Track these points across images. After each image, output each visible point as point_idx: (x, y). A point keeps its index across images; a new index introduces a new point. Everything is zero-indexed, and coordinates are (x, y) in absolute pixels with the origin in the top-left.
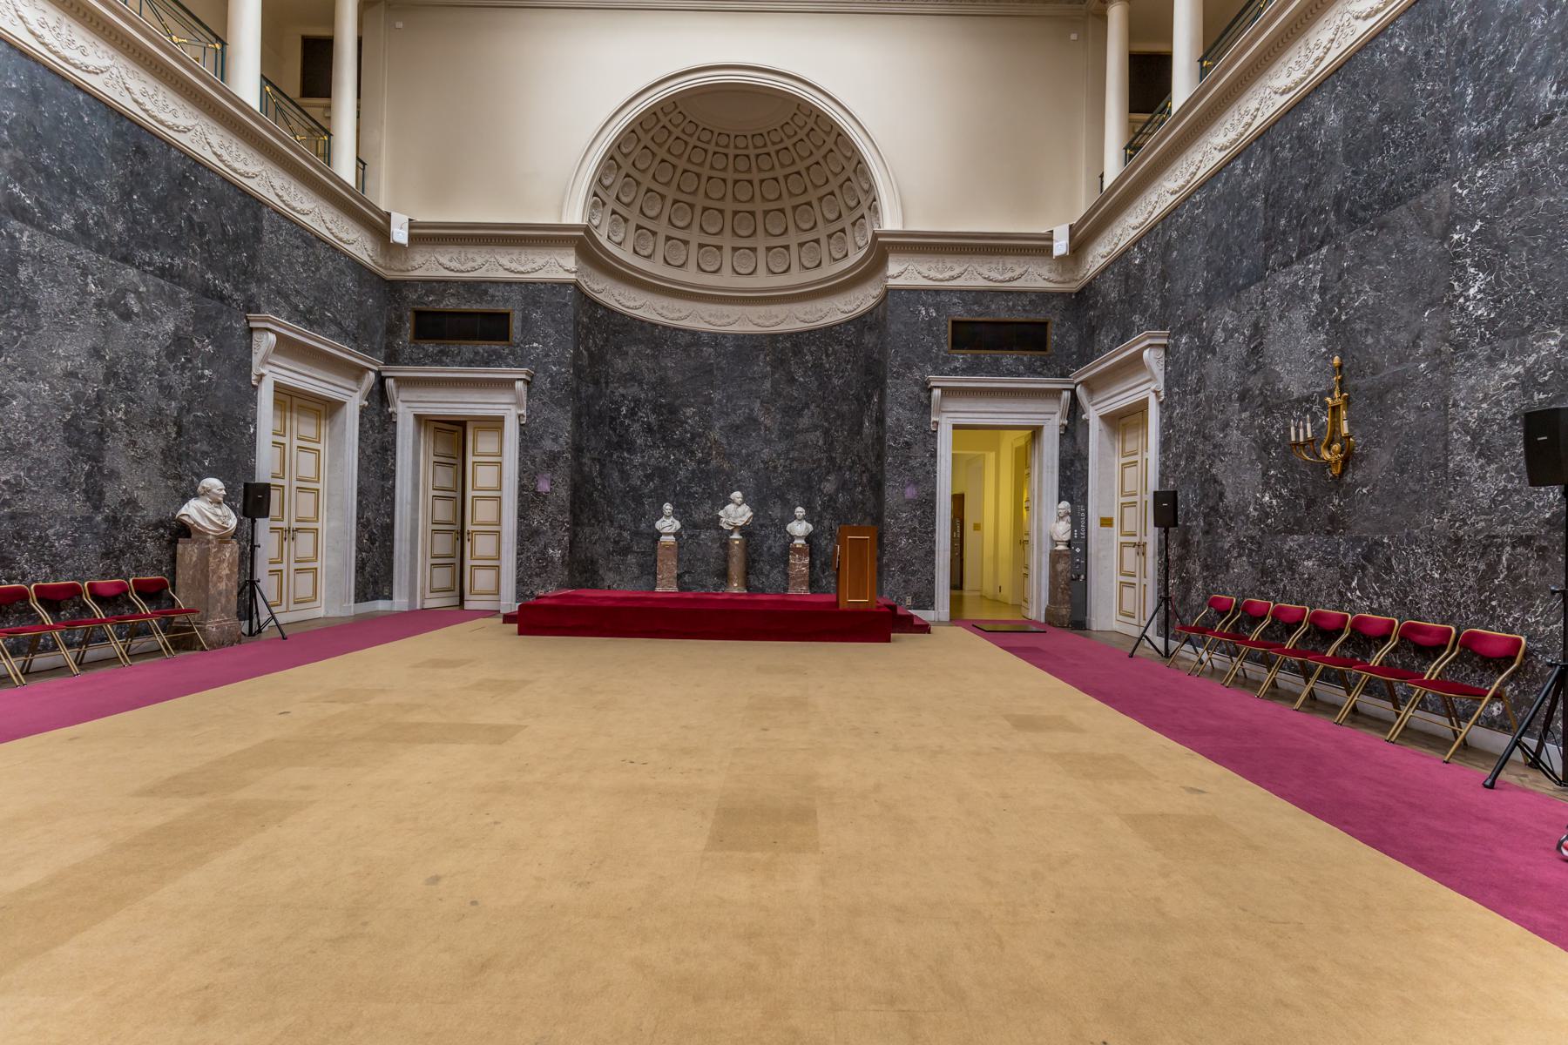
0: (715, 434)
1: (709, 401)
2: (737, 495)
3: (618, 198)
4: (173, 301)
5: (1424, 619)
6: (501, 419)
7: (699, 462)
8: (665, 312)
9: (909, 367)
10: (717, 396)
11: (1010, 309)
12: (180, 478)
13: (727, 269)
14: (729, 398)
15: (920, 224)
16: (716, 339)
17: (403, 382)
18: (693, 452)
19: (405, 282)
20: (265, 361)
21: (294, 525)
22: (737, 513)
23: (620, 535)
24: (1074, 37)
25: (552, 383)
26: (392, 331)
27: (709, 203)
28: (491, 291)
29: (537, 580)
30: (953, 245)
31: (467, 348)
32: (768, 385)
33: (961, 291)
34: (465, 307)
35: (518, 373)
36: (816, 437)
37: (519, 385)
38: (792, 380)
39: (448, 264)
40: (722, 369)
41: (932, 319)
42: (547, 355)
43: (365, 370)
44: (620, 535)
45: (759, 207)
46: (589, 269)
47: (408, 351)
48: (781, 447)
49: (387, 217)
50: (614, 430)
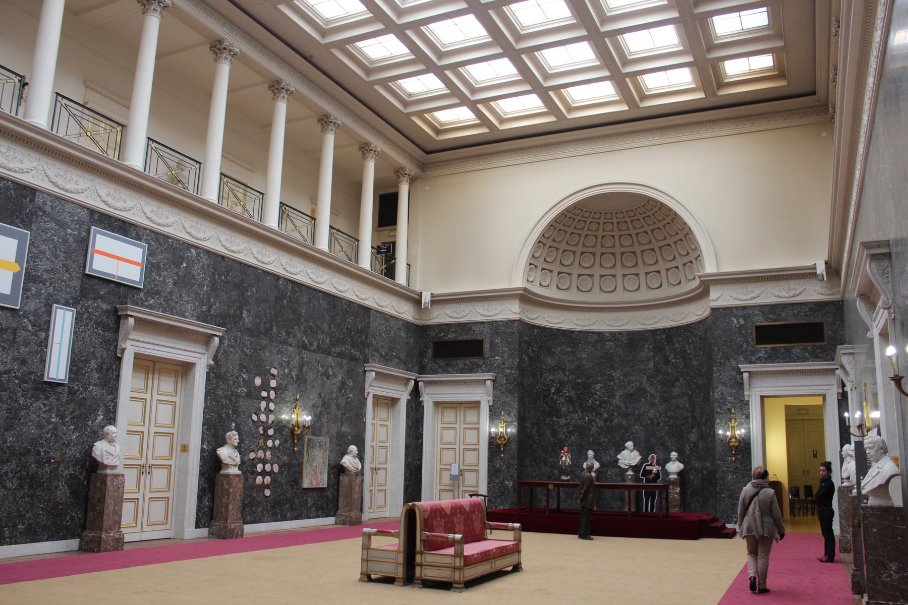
0: (616, 401)
1: (611, 378)
2: (629, 444)
3: (545, 260)
4: (341, 367)
5: (308, 454)
6: (478, 403)
7: (605, 421)
8: (579, 323)
9: (727, 358)
10: (617, 374)
11: (796, 315)
12: (341, 445)
13: (620, 288)
14: (625, 375)
15: (729, 267)
16: (615, 335)
17: (428, 383)
18: (601, 415)
19: (428, 326)
20: (371, 385)
21: (378, 466)
22: (629, 457)
23: (551, 472)
24: (824, 134)
25: (507, 380)
26: (422, 354)
27: (604, 250)
28: (473, 328)
29: (499, 500)
30: (752, 278)
31: (460, 363)
32: (651, 365)
33: (760, 306)
34: (460, 338)
35: (489, 376)
36: (684, 402)
37: (488, 382)
38: (667, 362)
39: (451, 315)
40: (620, 356)
41: (742, 326)
42: (504, 364)
43: (409, 380)
44: (551, 472)
45: (637, 248)
46: (528, 307)
47: (430, 365)
48: (662, 408)
49: (421, 295)
50: (547, 403)
